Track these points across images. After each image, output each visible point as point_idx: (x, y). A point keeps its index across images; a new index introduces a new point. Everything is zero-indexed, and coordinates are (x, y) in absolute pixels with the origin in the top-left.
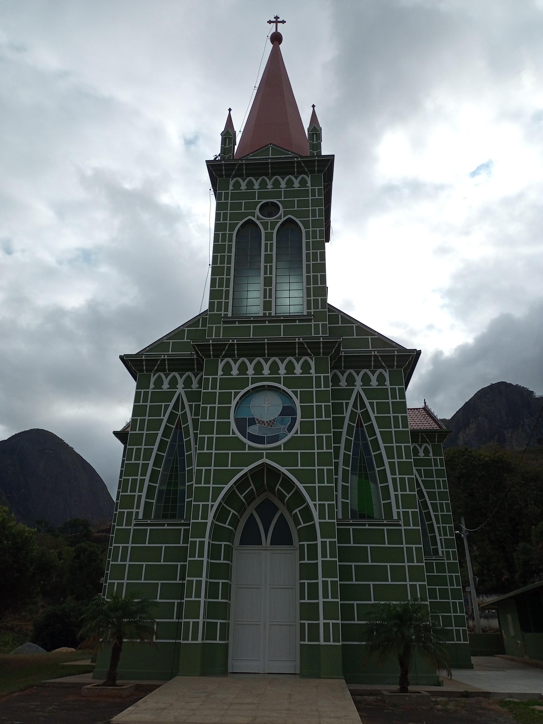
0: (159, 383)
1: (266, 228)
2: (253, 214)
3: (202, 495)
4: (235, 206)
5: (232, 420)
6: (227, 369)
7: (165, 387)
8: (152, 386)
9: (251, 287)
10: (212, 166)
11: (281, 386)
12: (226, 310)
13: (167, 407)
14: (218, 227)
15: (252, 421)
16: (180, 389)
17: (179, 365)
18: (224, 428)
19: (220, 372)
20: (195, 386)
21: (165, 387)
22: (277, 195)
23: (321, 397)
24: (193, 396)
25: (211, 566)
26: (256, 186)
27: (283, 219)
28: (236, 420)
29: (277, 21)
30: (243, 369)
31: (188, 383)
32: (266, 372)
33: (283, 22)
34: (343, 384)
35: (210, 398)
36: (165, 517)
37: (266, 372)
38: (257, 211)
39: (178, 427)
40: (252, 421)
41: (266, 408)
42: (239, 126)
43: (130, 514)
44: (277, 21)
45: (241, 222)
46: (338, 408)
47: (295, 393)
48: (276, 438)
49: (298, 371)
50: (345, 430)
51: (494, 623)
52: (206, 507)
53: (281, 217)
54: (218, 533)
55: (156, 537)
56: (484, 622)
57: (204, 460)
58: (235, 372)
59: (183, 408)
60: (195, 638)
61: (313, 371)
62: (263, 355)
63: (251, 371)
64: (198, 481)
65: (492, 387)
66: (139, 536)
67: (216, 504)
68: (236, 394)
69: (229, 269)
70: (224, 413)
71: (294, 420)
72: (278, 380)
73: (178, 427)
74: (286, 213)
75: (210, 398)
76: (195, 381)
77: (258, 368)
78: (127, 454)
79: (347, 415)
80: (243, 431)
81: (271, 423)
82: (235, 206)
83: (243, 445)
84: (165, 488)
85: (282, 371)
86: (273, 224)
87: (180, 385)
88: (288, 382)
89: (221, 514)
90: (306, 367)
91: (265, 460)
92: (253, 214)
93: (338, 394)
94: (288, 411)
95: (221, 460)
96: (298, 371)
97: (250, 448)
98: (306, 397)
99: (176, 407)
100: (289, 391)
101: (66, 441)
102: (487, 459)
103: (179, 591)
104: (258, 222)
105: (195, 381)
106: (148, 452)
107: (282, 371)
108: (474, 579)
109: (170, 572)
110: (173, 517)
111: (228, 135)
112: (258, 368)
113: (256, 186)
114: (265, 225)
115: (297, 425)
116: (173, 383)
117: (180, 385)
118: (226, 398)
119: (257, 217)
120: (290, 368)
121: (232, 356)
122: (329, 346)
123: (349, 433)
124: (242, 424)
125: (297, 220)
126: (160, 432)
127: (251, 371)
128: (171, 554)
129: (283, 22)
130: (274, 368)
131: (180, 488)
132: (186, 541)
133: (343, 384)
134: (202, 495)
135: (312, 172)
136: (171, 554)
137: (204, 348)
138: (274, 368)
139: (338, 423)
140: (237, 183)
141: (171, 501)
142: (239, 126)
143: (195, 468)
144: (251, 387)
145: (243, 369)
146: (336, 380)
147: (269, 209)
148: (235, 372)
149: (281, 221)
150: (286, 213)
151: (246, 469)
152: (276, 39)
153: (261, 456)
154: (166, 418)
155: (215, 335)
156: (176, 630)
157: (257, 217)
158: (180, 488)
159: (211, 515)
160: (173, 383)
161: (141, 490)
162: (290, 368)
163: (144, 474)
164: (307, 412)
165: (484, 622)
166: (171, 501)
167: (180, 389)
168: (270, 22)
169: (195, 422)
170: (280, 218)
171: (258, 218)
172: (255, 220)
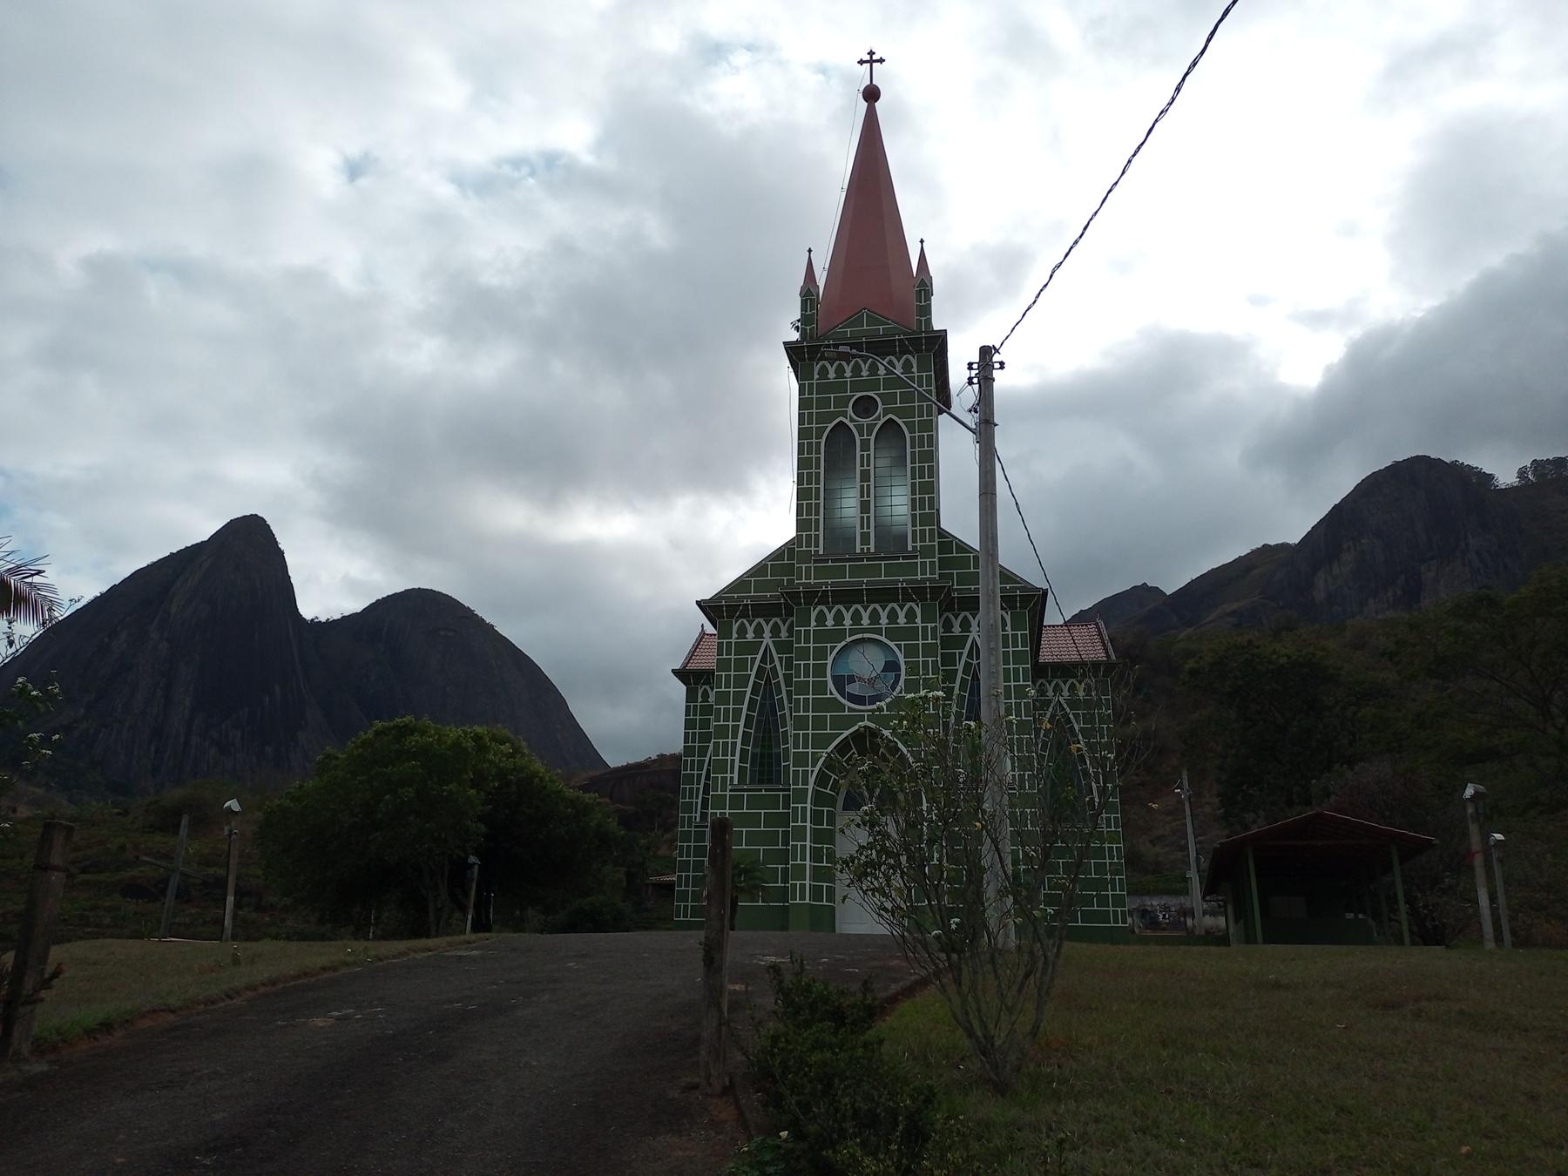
0: (742, 631)
1: (861, 435)
2: (845, 414)
3: (801, 760)
4: (823, 403)
5: (829, 678)
6: (821, 618)
7: (750, 636)
8: (735, 635)
9: (846, 493)
10: (790, 348)
11: (883, 639)
12: (817, 545)
13: (753, 660)
14: (803, 433)
15: (851, 679)
16: (767, 639)
17: (763, 610)
18: (821, 687)
19: (813, 623)
20: (784, 634)
21: (750, 636)
22: (874, 385)
23: (929, 650)
24: (784, 647)
25: (815, 832)
26: (848, 374)
27: (883, 420)
28: (833, 677)
29: (872, 60)
30: (839, 618)
31: (775, 631)
32: (865, 621)
33: (881, 61)
34: (957, 630)
35: (804, 653)
36: (761, 782)
37: (865, 621)
38: (850, 410)
39: (768, 682)
40: (851, 679)
41: (866, 663)
42: (821, 278)
43: (724, 779)
44: (872, 60)
45: (831, 426)
46: (949, 660)
47: (899, 646)
48: (879, 698)
49: (902, 620)
50: (957, 685)
51: (1222, 921)
52: (805, 773)
53: (880, 417)
54: (819, 798)
55: (754, 802)
56: (1209, 921)
57: (801, 723)
58: (830, 622)
59: (772, 661)
60: (803, 897)
61: (918, 620)
62: (861, 602)
63: (848, 622)
64: (796, 746)
65: (1396, 470)
66: (736, 802)
67: (816, 770)
68: (833, 648)
69: (818, 459)
70: (819, 670)
71: (898, 677)
72: (879, 631)
73: (768, 682)
74: (886, 412)
75: (804, 653)
76: (784, 629)
77: (857, 618)
78: (691, 696)
79: (960, 667)
80: (841, 691)
81: (871, 681)
82: (823, 403)
83: (842, 707)
84: (758, 750)
85: (884, 620)
86: (871, 427)
87: (767, 634)
88: (891, 634)
89: (822, 779)
90: (911, 616)
91: (866, 723)
92: (845, 414)
93: (948, 642)
94: (891, 666)
95: (819, 723)
96: (902, 620)
97: (850, 709)
98: (910, 652)
99: (763, 660)
100: (892, 644)
101: (506, 629)
102: (1283, 660)
103: (784, 857)
104: (851, 425)
105: (784, 629)
106: (738, 713)
107: (884, 620)
108: (1198, 859)
109: (771, 838)
110: (770, 781)
111: (808, 295)
112: (857, 618)
113: (848, 374)
114: (860, 428)
115: (902, 682)
116: (759, 631)
117: (767, 634)
118: (821, 654)
119: (850, 418)
120: (893, 616)
121: (826, 603)
122: (936, 591)
123: (962, 688)
124: (840, 682)
125: (899, 421)
126: (749, 690)
127: (848, 622)
128: (772, 820)
129: (881, 61)
130: (875, 617)
131: (775, 750)
132: (787, 806)
133: (957, 630)
134: (801, 760)
135: (919, 351)
136: (772, 820)
137: (794, 596)
138: (875, 617)
139: (950, 676)
140: (824, 369)
141: (766, 765)
142: (821, 278)
143: (792, 732)
144: (849, 639)
145: (839, 618)
146: (948, 626)
147: (865, 407)
148: (830, 622)
149: (880, 423)
150: (886, 412)
151: (847, 733)
152: (871, 94)
153: (862, 718)
154: (753, 674)
155: (807, 579)
156: (783, 894)
157: (850, 418)
158: (775, 750)
159: (812, 780)
160: (759, 631)
161: (733, 754)
162: (893, 616)
163: (735, 736)
164: (913, 669)
165: (1209, 921)
166: (766, 765)
167: (767, 639)
168: (861, 62)
169: (788, 679)
170: (878, 418)
171: (852, 420)
172: (847, 421)
